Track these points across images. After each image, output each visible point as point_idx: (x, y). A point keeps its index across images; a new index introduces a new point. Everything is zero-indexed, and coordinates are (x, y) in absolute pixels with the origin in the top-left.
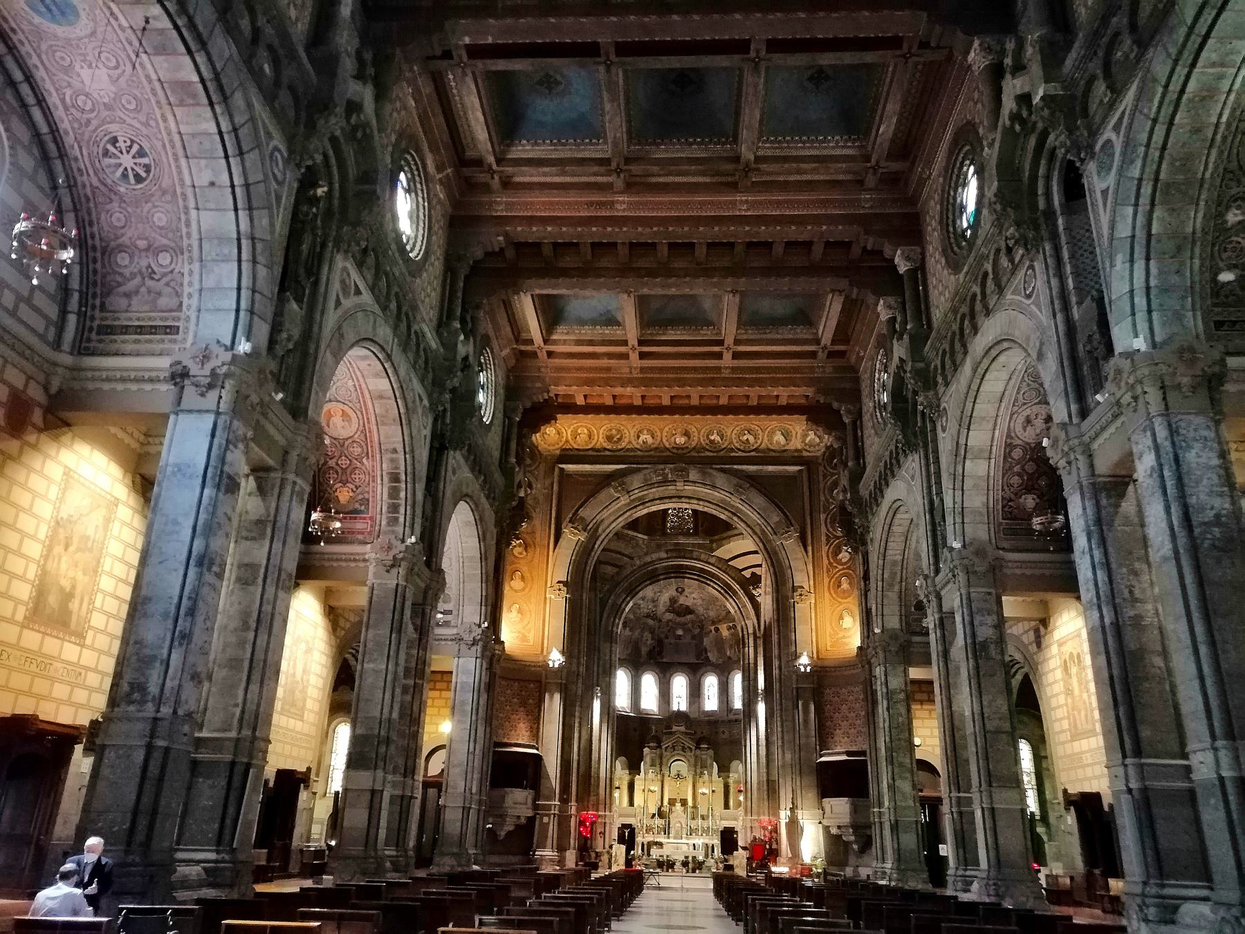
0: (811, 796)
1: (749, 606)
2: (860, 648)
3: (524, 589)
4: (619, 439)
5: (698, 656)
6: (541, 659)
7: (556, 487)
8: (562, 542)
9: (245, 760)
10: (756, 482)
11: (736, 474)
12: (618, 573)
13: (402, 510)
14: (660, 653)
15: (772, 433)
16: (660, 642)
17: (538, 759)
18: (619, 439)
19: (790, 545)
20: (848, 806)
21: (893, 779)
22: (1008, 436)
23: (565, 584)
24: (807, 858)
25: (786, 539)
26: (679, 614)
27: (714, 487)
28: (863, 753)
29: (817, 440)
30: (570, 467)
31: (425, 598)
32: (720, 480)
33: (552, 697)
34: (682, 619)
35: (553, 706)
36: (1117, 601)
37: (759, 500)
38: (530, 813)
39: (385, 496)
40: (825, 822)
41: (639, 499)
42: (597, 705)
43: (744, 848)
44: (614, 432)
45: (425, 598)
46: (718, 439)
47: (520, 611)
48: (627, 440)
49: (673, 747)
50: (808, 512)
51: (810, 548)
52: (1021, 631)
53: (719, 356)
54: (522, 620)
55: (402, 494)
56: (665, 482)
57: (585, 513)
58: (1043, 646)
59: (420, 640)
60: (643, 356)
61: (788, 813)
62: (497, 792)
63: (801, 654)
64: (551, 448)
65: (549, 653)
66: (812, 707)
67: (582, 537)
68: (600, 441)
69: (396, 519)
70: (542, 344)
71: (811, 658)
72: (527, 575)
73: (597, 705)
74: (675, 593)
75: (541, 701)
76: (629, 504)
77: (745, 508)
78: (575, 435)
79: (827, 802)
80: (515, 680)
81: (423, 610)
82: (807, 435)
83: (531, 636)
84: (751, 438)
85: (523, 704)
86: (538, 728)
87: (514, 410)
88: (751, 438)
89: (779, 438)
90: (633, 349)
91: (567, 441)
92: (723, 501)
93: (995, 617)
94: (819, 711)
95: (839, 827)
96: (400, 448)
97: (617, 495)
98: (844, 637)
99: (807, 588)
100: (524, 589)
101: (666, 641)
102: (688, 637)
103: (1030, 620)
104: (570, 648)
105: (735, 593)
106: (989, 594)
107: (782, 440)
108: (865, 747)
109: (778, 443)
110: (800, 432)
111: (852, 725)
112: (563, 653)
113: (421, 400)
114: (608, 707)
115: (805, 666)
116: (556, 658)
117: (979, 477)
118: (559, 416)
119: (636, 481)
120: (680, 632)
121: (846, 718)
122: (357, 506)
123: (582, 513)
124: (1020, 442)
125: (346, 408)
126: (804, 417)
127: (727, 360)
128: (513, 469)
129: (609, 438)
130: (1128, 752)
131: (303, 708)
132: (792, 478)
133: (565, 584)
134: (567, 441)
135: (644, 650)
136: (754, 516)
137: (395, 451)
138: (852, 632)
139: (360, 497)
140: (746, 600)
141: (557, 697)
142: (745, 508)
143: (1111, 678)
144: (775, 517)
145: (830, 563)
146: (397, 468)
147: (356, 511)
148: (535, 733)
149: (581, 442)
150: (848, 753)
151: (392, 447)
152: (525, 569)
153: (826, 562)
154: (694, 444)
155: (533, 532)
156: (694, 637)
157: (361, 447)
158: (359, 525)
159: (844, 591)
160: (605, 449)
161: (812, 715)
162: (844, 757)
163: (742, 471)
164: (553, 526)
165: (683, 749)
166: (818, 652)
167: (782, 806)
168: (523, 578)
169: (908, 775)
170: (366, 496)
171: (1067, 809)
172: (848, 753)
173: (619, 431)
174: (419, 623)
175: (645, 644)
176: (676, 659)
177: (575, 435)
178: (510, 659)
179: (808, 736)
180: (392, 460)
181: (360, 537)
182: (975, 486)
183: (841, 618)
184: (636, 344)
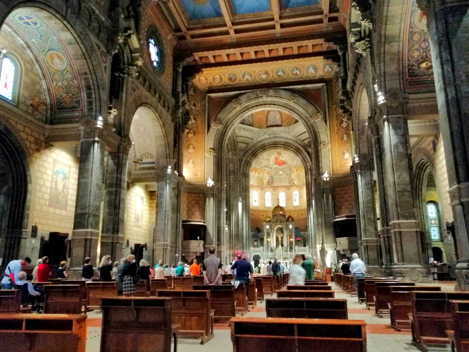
0: (330, 238)
1: (308, 157)
2: (351, 167)
3: (194, 153)
4: (235, 79)
5: (290, 182)
6: (204, 183)
7: (207, 105)
8: (211, 130)
9: (116, 241)
10: (304, 94)
11: (292, 91)
12: (247, 147)
13: (94, 104)
14: (272, 182)
15: (308, 68)
16: (272, 177)
17: (204, 227)
18: (235, 79)
19: (318, 121)
20: (347, 241)
21: (365, 226)
22: (411, 27)
23: (213, 149)
24: (328, 265)
25: (316, 119)
26: (280, 165)
27: (281, 97)
28: (354, 216)
29: (330, 70)
30: (213, 95)
31: (119, 149)
32: (283, 93)
33: (209, 199)
34: (281, 167)
35: (210, 204)
36: (458, 82)
37: (302, 101)
38: (202, 250)
39: (85, 98)
40: (338, 249)
41: (246, 107)
42: (240, 205)
43: (61, 212)
44: (232, 76)
45: (119, 149)
46: (282, 74)
47: (193, 163)
48: (238, 79)
49: (276, 221)
50: (326, 105)
51: (328, 122)
52: (426, 145)
53: (273, 27)
54: (194, 167)
55: (93, 96)
56: (257, 97)
57: (221, 116)
58: (437, 149)
59: (118, 169)
60: (236, 31)
61: (321, 246)
62: (186, 242)
63: (325, 172)
64: (204, 87)
65: (207, 180)
66: (330, 196)
67: (220, 127)
68: (225, 81)
69: (92, 108)
70: (186, 31)
71: (329, 174)
72: (196, 146)
73: (240, 205)
74: (277, 155)
75: (205, 201)
76: (241, 110)
77: (296, 107)
78: (214, 79)
79: (338, 239)
80: (193, 193)
81: (118, 155)
82: (325, 68)
83: (199, 174)
84: (298, 72)
85: (198, 203)
86: (204, 214)
87: (179, 66)
88: (298, 72)
89: (312, 71)
90: (230, 28)
91: (211, 83)
92: (286, 104)
93: (403, 130)
94: (333, 199)
95: (344, 251)
96: (88, 72)
97: (235, 106)
98: (345, 163)
99: (327, 141)
100: (194, 153)
101: (275, 177)
102: (285, 174)
103: (429, 136)
104: (218, 177)
105: (301, 151)
106: (399, 118)
107: (313, 71)
108: (355, 213)
109: (311, 73)
110: (322, 66)
111: (350, 204)
112: (213, 180)
113: (99, 48)
114: (246, 206)
115: (326, 178)
116: (210, 183)
117: (394, 54)
118: (203, 69)
119: (243, 98)
120: (281, 173)
121: (347, 201)
122: (74, 104)
123: (219, 116)
124: (417, 30)
125: (58, 53)
126: (322, 57)
127: (278, 29)
128: (179, 94)
129: (230, 79)
130: (462, 179)
131: (66, 204)
132: (319, 90)
133: (213, 149)
134: (211, 83)
135: (265, 182)
136: (301, 110)
137: (86, 73)
138: (348, 160)
139: (75, 100)
140: (306, 154)
141: (212, 199)
142: (296, 107)
143: (452, 134)
144: (311, 109)
145: (338, 129)
146: (89, 82)
147: (74, 107)
148: (203, 216)
149: (217, 83)
150: (347, 217)
151: (83, 72)
152: (195, 144)
153: (336, 128)
154: (271, 78)
155: (198, 127)
156: (287, 175)
157: (72, 74)
158: (77, 114)
159: (345, 141)
160: (229, 85)
161: (330, 201)
162: (345, 218)
163: (295, 89)
164: (206, 123)
165: (281, 222)
166: (333, 171)
167: (318, 243)
168: (194, 148)
169: (373, 224)
170: (78, 99)
171: (448, 233)
172: (347, 217)
173: (234, 75)
174: (116, 161)
175: (265, 179)
176: (280, 184)
177: (214, 79)
178: (189, 184)
179: (328, 210)
180: (86, 79)
181: (77, 119)
182: (392, 59)
183: (344, 154)
184: (231, 25)
